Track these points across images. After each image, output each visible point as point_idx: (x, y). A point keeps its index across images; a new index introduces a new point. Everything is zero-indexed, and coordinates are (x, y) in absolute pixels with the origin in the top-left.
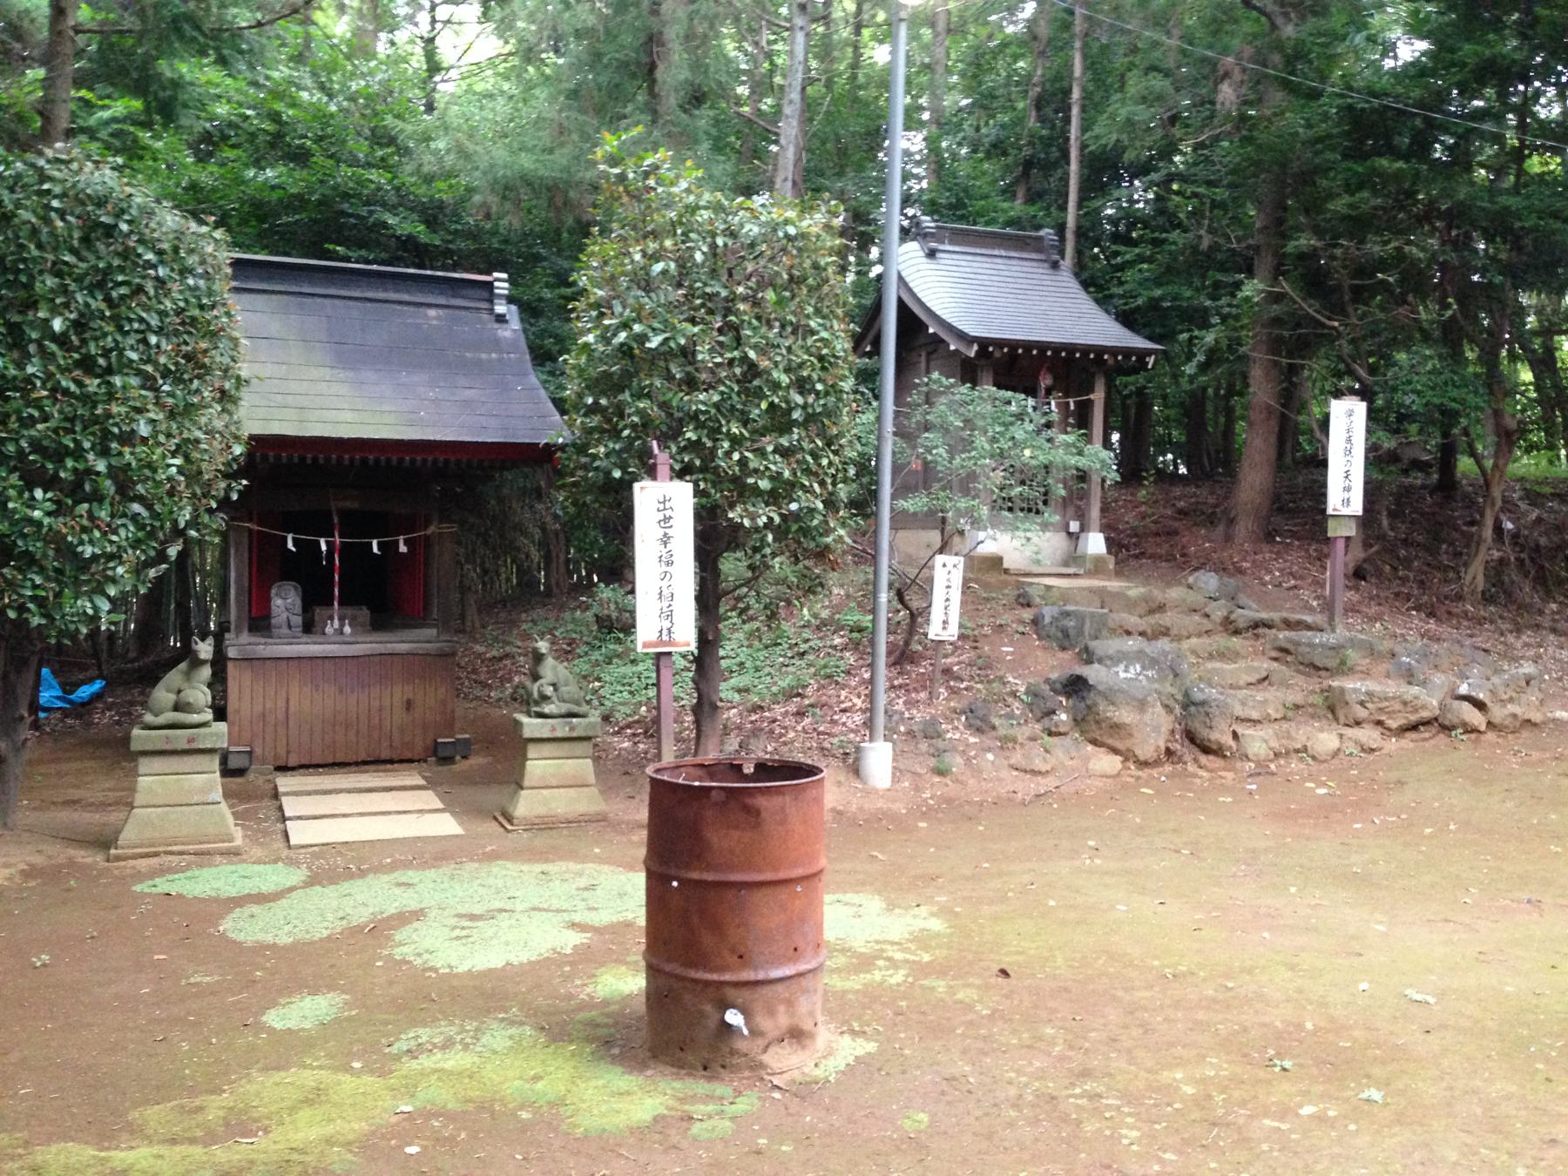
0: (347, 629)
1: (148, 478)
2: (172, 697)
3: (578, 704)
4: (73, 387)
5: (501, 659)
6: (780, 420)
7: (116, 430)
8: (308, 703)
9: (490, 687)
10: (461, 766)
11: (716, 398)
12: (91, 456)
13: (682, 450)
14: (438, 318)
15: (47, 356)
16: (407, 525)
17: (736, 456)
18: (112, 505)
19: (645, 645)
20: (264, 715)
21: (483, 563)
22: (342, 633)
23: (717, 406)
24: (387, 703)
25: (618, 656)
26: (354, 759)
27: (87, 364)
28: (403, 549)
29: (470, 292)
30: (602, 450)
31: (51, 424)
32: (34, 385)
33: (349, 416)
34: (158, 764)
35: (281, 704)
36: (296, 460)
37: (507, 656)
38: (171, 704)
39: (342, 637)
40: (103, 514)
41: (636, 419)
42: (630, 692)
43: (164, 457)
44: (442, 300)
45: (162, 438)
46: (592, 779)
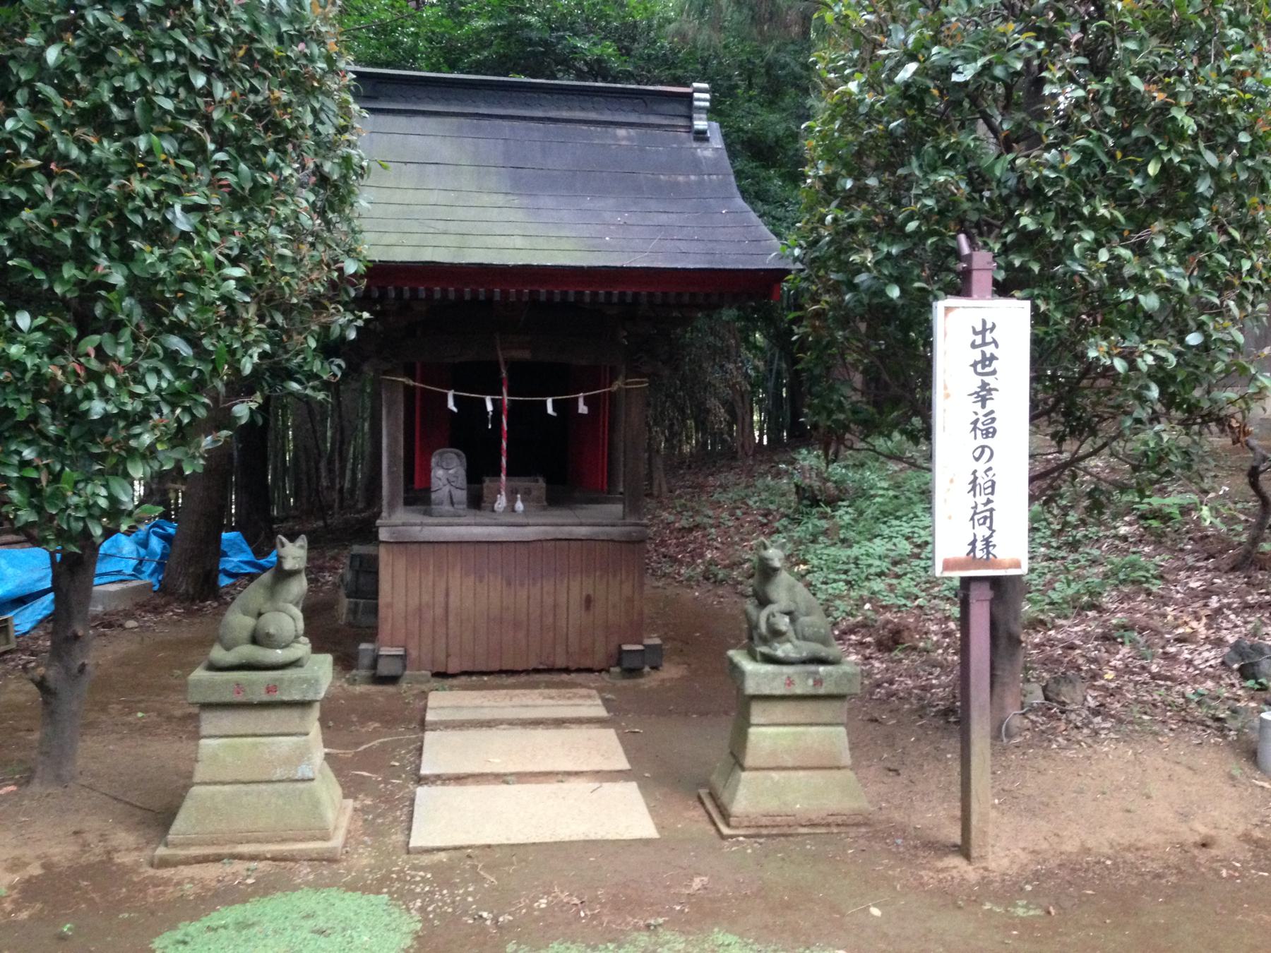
0: (519, 506)
1: (193, 297)
2: (249, 622)
3: (824, 642)
4: (75, 153)
5: (690, 530)
6: (1175, 195)
7: (138, 220)
8: (469, 596)
9: (681, 563)
10: (650, 681)
11: (1073, 159)
12: (103, 262)
13: (1006, 249)
14: (629, 138)
15: (39, 105)
16: (590, 378)
17: (1104, 255)
18: (136, 339)
19: (948, 565)
20: (420, 609)
21: (672, 425)
22: (513, 511)
23: (1073, 171)
24: (562, 599)
25: (825, 533)
26: (524, 667)
27: (97, 119)
28: (583, 409)
29: (667, 108)
30: (870, 256)
31: (45, 209)
32: (16, 149)
33: (519, 242)
34: (227, 721)
35: (440, 598)
36: (452, 296)
37: (697, 526)
38: (246, 634)
39: (514, 517)
40: (121, 352)
41: (930, 202)
42: (848, 582)
43: (219, 265)
44: (633, 118)
45: (213, 236)
46: (846, 759)
